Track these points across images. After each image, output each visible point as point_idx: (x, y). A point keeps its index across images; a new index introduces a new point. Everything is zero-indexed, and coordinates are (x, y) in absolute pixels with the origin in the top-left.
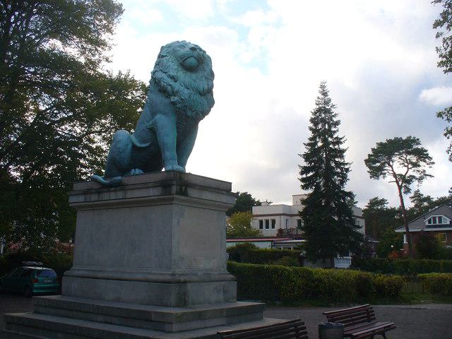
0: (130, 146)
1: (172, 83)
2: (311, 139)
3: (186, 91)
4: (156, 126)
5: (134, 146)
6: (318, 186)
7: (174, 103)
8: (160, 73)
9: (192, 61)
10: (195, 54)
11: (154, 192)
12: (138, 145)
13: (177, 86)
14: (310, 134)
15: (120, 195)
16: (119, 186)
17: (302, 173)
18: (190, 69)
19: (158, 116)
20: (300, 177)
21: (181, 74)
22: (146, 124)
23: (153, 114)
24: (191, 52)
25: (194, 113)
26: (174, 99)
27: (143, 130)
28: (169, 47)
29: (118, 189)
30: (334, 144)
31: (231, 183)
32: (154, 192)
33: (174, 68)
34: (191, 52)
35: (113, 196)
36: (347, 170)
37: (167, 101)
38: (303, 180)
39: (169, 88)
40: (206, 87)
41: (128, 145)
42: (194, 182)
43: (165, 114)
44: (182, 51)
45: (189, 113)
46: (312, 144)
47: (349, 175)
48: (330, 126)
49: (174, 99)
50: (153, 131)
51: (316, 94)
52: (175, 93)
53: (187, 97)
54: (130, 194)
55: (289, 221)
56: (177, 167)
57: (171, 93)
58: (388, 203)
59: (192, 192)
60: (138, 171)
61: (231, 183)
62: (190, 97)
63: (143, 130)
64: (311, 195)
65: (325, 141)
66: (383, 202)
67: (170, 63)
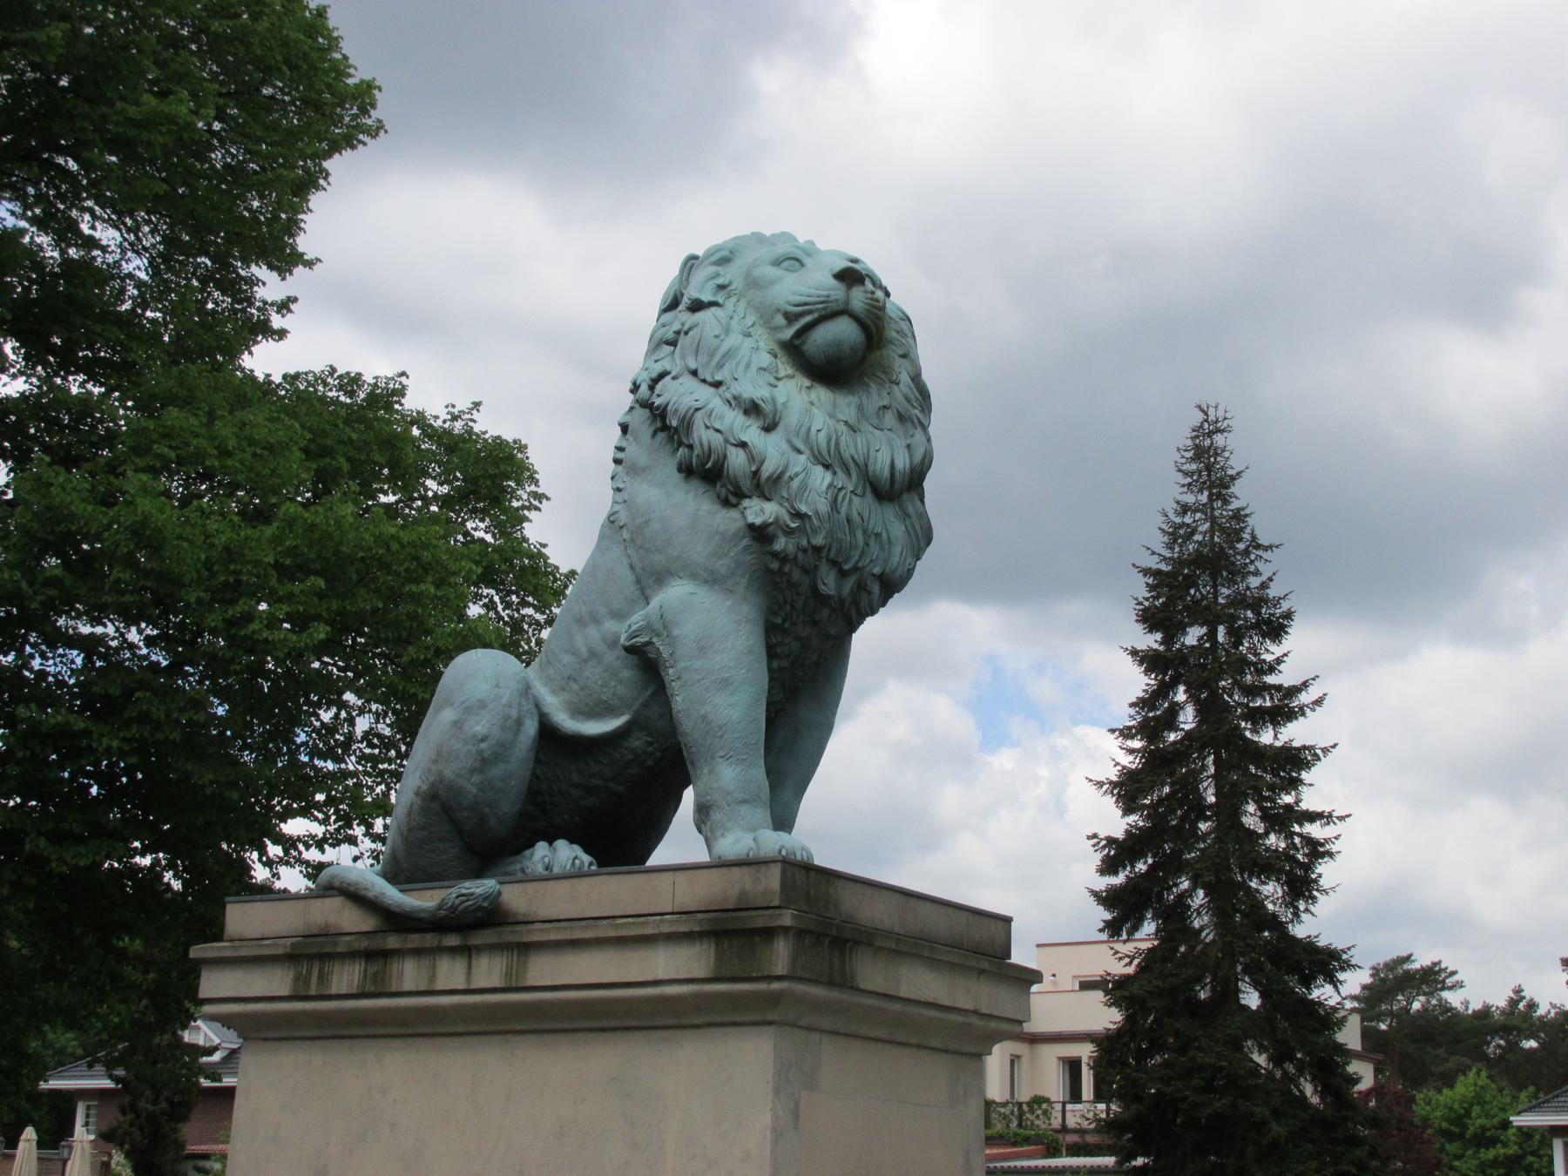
0: (531, 728)
1: (752, 433)
2: (1142, 704)
3: (821, 478)
4: (671, 640)
5: (548, 734)
6: (1174, 918)
7: (760, 534)
8: (688, 382)
9: (842, 331)
10: (858, 298)
11: (674, 966)
12: (567, 723)
13: (773, 450)
14: (1139, 682)
15: (489, 971)
16: (475, 927)
17: (1109, 867)
18: (832, 372)
19: (676, 593)
20: (1104, 883)
21: (798, 398)
22: (611, 626)
23: (649, 579)
24: (837, 290)
25: (849, 584)
26: (760, 511)
27: (593, 654)
28: (724, 261)
29: (477, 939)
30: (1259, 717)
31: (1007, 921)
32: (674, 966)
33: (755, 366)
34: (837, 290)
35: (450, 973)
36: (1317, 850)
37: (728, 520)
38: (1108, 899)
39: (737, 460)
40: (902, 462)
41: (519, 723)
42: (872, 913)
43: (712, 580)
44: (792, 289)
45: (829, 582)
46: (1152, 720)
47: (1326, 872)
48: (1236, 635)
49: (760, 511)
50: (646, 662)
51: (1164, 489)
52: (764, 486)
53: (823, 506)
54: (545, 970)
55: (1025, 1061)
56: (772, 841)
57: (746, 485)
58: (1459, 985)
59: (872, 974)
60: (566, 853)
61: (1007, 921)
62: (834, 504)
63: (593, 654)
64: (1151, 961)
65: (1210, 709)
66: (1432, 978)
67: (734, 339)
